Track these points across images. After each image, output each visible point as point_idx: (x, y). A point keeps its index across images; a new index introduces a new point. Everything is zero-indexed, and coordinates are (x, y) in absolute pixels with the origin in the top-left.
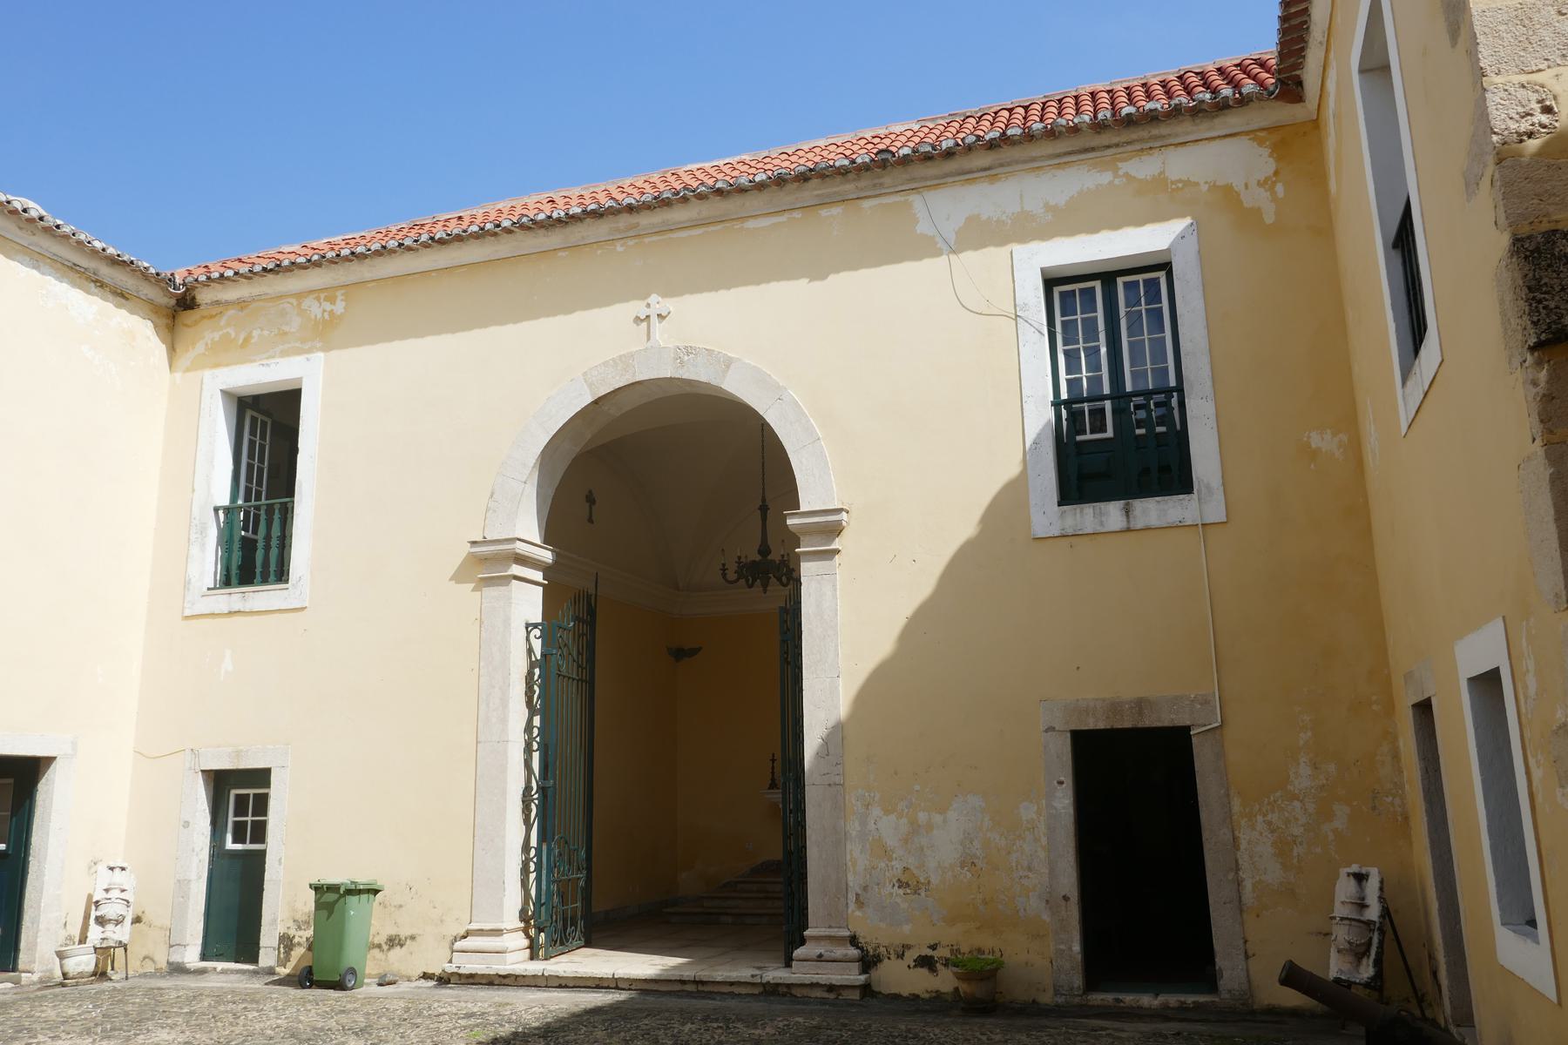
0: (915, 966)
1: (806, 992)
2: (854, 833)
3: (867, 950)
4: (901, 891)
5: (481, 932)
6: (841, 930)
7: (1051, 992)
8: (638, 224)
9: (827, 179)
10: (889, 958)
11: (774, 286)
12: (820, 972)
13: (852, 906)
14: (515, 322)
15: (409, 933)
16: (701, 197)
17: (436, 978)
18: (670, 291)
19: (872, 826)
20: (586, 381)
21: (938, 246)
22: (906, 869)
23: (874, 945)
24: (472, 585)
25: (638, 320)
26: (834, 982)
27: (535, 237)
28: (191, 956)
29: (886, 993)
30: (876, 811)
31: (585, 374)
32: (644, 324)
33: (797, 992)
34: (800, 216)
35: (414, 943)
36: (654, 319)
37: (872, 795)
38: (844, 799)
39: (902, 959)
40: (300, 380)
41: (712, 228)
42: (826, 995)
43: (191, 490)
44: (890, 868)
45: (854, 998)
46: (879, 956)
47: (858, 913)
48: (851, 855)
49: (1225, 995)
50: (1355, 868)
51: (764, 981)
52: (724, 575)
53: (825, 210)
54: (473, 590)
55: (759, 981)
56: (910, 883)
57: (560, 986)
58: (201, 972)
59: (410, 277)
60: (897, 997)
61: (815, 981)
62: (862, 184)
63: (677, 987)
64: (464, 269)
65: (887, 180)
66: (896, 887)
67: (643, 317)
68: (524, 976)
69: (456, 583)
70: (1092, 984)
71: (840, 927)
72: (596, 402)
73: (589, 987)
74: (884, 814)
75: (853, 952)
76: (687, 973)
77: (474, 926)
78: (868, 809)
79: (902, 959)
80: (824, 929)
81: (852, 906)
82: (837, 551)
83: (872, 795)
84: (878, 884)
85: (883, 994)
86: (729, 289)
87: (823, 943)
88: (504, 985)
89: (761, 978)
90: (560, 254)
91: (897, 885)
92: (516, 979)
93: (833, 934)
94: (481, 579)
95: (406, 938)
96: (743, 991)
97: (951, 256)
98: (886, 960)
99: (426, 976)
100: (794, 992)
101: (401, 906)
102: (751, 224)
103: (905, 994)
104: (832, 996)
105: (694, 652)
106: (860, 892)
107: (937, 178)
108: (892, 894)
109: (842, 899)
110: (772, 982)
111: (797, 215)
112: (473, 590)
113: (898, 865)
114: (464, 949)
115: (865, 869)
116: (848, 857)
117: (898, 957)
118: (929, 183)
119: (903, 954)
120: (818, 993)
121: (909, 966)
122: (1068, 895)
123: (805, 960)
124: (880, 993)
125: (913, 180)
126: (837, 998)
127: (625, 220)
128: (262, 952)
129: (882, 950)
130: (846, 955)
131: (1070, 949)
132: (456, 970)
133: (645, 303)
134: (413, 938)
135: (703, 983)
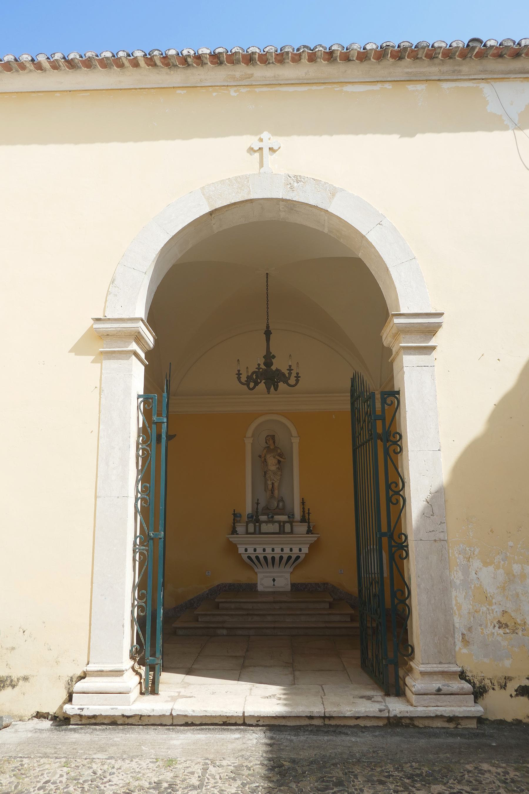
0: (517, 695)
2: (458, 582)
3: (474, 682)
4: (501, 631)
5: (100, 673)
6: (451, 666)
8: (251, 76)
9: (418, 60)
10: (493, 689)
11: (370, 136)
12: (439, 704)
13: (459, 644)
14: (136, 141)
15: (21, 674)
16: (313, 58)
17: (50, 717)
18: (277, 132)
19: (473, 576)
20: (204, 195)
21: (505, 123)
22: (504, 612)
23: (480, 678)
24: (92, 358)
25: (251, 150)
26: (457, 714)
27: (158, 73)
29: (493, 720)
30: (476, 564)
31: (203, 188)
32: (257, 155)
33: (419, 723)
34: (391, 87)
35: (27, 684)
36: (266, 151)
37: (472, 549)
38: (449, 552)
39: (505, 689)
41: (314, 88)
42: (446, 725)
44: (491, 612)
45: (472, 726)
46: (484, 687)
47: (465, 651)
48: (456, 600)
52: (239, 379)
53: (412, 86)
54: (92, 362)
55: (387, 715)
56: (508, 624)
57: (186, 724)
59: (33, 95)
60: (501, 723)
61: (439, 713)
62: (445, 68)
63: (306, 722)
64: (88, 94)
65: (465, 69)
66: (497, 628)
67: (256, 148)
68: (149, 716)
69: (76, 355)
71: (449, 663)
72: (211, 213)
73: (216, 724)
74: (484, 566)
75: (467, 686)
77: (92, 667)
78: (469, 561)
79: (505, 689)
80: (435, 665)
81: (459, 644)
82: (433, 348)
83: (472, 549)
84: (481, 625)
85: (490, 720)
86: (331, 135)
88: (128, 724)
89: (389, 712)
90: (179, 91)
91: (497, 626)
92: (140, 719)
93: (446, 670)
94: (101, 352)
95: (18, 680)
96: (369, 723)
97: (516, 131)
98: (491, 691)
99: (39, 716)
101: (13, 648)
102: (349, 88)
103: (509, 719)
104: (452, 725)
105: (174, 436)
106: (465, 632)
107: (503, 73)
108: (493, 634)
109: (450, 639)
110: (398, 716)
111: (388, 86)
112: (92, 362)
113: (497, 609)
114: (85, 690)
115: (469, 613)
116: (454, 602)
117: (501, 688)
118: (495, 76)
119: (505, 685)
120: (439, 724)
121: (511, 696)
123: (424, 694)
124: (487, 719)
125: (484, 71)
126: (456, 728)
127: (242, 70)
129: (487, 682)
132: (78, 712)
133: (258, 137)
134: (26, 679)
135: (330, 718)
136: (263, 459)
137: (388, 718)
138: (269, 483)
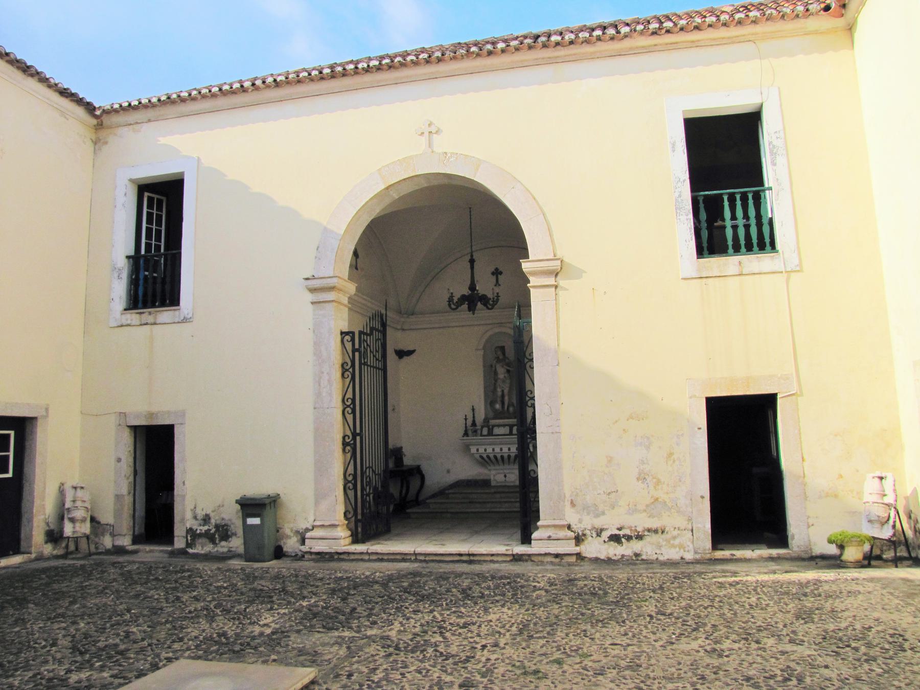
1: (540, 558)
7: (692, 553)
28: (125, 541)
40: (182, 174)
43: (694, 532)
49: (795, 549)
50: (878, 474)
51: (514, 553)
58: (135, 552)
61: (547, 552)
68: (82, 385)
70: (715, 547)
75: (572, 535)
76: (464, 550)
87: (550, 529)
96: (500, 559)
100: (533, 559)
104: (557, 560)
122: (704, 495)
128: (176, 539)
130: (566, 536)
131: (704, 527)
132: (309, 550)
135: (473, 555)
136: (493, 369)
137: (513, 555)
138: (499, 390)
